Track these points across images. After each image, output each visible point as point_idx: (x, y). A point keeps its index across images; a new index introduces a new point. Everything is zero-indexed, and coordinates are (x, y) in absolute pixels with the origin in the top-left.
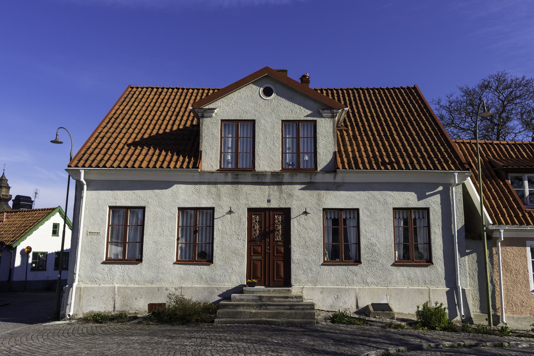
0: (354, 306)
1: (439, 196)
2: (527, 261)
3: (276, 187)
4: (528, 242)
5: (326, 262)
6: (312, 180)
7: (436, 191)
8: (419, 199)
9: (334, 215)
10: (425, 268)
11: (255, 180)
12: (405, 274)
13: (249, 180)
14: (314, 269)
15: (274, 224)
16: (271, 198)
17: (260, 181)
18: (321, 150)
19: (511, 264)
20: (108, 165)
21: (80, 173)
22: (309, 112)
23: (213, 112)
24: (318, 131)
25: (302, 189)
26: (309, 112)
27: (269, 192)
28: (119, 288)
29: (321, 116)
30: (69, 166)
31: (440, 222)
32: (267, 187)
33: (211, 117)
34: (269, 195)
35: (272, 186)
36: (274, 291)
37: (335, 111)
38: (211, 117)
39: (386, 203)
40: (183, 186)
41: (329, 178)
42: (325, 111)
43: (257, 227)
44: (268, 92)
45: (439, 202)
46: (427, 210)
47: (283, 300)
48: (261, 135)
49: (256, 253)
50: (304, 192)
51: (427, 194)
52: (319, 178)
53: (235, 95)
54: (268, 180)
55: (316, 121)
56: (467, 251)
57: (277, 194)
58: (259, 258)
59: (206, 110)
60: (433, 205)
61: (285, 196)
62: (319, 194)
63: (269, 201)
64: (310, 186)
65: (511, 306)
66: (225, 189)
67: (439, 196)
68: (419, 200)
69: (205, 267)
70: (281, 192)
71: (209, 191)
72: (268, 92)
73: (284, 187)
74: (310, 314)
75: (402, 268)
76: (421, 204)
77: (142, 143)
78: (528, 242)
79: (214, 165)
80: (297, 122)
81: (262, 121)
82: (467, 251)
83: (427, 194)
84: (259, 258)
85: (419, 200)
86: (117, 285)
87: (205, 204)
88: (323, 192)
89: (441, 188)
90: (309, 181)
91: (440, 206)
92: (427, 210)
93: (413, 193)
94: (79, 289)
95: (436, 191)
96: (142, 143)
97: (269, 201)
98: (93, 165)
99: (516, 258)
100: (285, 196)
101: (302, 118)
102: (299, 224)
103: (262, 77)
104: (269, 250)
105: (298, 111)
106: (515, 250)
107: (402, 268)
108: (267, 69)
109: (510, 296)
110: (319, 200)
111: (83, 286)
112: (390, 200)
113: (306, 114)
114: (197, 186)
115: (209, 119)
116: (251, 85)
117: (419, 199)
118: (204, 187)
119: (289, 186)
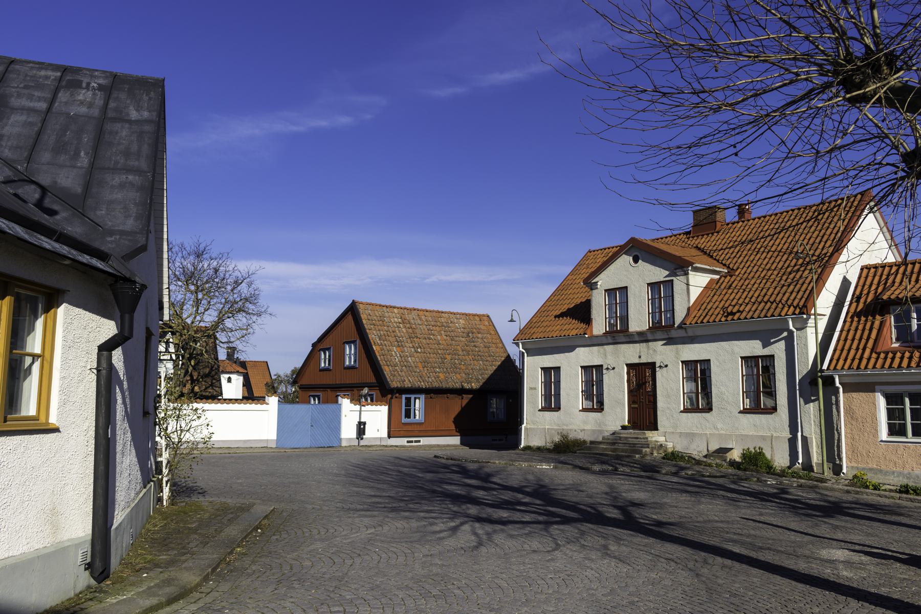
0: (706, 450)
1: (783, 342)
2: (876, 408)
3: (644, 344)
4: (877, 387)
5: (687, 409)
6: (670, 336)
7: (781, 337)
8: (764, 346)
9: (766, 363)
10: (770, 416)
11: (628, 340)
12: (751, 420)
13: (624, 340)
14: (675, 416)
15: (645, 377)
16: (642, 354)
17: (631, 340)
18: (677, 307)
19: (857, 412)
20: (705, 321)
21: (788, 322)
22: (667, 273)
23: (597, 285)
24: (674, 289)
25: (664, 345)
26: (667, 273)
27: (640, 349)
28: (548, 429)
29: (676, 275)
30: (514, 340)
31: (785, 369)
32: (638, 345)
33: (597, 288)
34: (640, 352)
35: (641, 344)
36: (634, 433)
37: (685, 269)
38: (597, 288)
39: (733, 353)
40: (582, 349)
41: (681, 333)
42: (678, 270)
43: (634, 379)
44: (636, 260)
45: (784, 348)
46: (772, 357)
47: (635, 440)
48: (632, 299)
49: (634, 402)
50: (665, 347)
51: (772, 341)
52: (674, 334)
53: (612, 268)
54: (637, 338)
55: (673, 280)
56: (813, 398)
57: (646, 350)
58: (636, 406)
59: (594, 283)
60: (777, 351)
61: (651, 351)
62: (677, 349)
63: (640, 357)
64: (670, 341)
65: (856, 455)
66: (609, 348)
67: (783, 342)
68: (764, 347)
69: (599, 414)
70: (648, 348)
71: (599, 351)
72: (636, 260)
73: (650, 343)
74: (639, 450)
75: (748, 415)
76: (767, 351)
77: (562, 315)
78: (877, 387)
79: (600, 329)
80: (658, 284)
81: (632, 287)
82: (813, 398)
83: (772, 341)
84: (636, 406)
85: (764, 347)
86: (547, 427)
87: (597, 362)
88: (680, 346)
89: (785, 334)
90: (667, 337)
91: (785, 352)
92: (772, 357)
93: (758, 342)
94: (526, 429)
95: (781, 337)
96: (562, 315)
97: (640, 357)
98: (769, 315)
99: (863, 405)
100: (651, 351)
101: (662, 279)
102: (662, 375)
103: (629, 248)
104: (643, 399)
105: (659, 273)
106: (859, 397)
107: (748, 415)
108: (633, 240)
109: (856, 446)
110: (677, 353)
111: (529, 426)
112: (736, 350)
113: (665, 275)
114: (591, 348)
115: (596, 290)
116: (624, 255)
117: (764, 346)
118: (595, 348)
119: (654, 343)
